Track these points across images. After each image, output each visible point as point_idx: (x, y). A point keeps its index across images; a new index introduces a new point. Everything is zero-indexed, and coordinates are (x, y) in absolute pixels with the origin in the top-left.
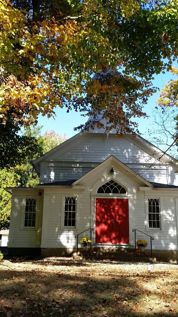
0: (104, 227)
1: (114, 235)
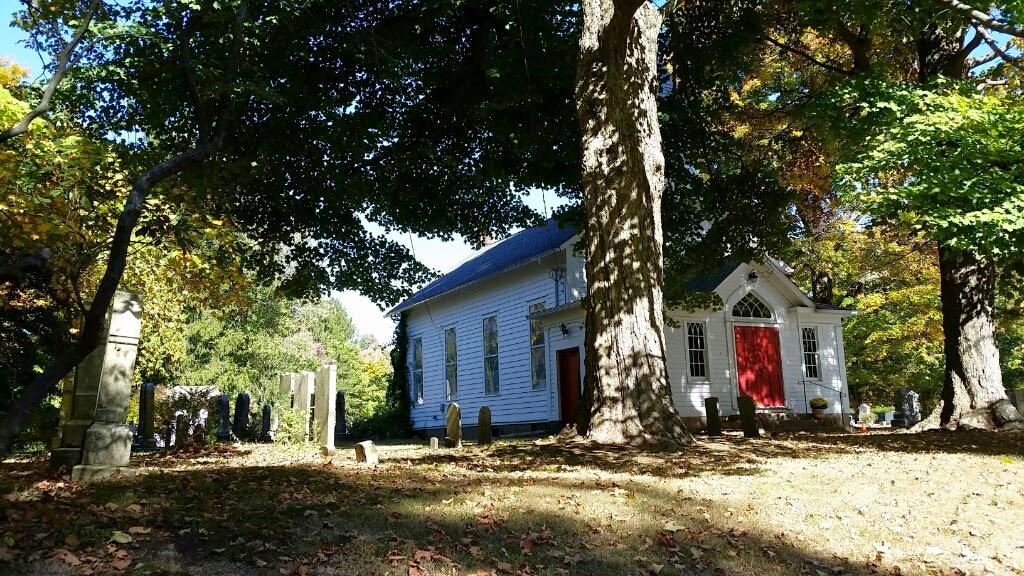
0: (750, 375)
1: (764, 392)
